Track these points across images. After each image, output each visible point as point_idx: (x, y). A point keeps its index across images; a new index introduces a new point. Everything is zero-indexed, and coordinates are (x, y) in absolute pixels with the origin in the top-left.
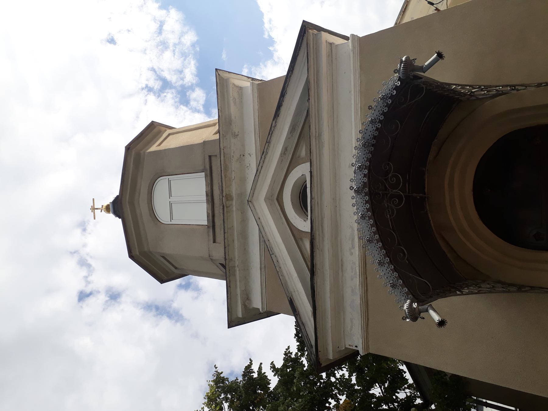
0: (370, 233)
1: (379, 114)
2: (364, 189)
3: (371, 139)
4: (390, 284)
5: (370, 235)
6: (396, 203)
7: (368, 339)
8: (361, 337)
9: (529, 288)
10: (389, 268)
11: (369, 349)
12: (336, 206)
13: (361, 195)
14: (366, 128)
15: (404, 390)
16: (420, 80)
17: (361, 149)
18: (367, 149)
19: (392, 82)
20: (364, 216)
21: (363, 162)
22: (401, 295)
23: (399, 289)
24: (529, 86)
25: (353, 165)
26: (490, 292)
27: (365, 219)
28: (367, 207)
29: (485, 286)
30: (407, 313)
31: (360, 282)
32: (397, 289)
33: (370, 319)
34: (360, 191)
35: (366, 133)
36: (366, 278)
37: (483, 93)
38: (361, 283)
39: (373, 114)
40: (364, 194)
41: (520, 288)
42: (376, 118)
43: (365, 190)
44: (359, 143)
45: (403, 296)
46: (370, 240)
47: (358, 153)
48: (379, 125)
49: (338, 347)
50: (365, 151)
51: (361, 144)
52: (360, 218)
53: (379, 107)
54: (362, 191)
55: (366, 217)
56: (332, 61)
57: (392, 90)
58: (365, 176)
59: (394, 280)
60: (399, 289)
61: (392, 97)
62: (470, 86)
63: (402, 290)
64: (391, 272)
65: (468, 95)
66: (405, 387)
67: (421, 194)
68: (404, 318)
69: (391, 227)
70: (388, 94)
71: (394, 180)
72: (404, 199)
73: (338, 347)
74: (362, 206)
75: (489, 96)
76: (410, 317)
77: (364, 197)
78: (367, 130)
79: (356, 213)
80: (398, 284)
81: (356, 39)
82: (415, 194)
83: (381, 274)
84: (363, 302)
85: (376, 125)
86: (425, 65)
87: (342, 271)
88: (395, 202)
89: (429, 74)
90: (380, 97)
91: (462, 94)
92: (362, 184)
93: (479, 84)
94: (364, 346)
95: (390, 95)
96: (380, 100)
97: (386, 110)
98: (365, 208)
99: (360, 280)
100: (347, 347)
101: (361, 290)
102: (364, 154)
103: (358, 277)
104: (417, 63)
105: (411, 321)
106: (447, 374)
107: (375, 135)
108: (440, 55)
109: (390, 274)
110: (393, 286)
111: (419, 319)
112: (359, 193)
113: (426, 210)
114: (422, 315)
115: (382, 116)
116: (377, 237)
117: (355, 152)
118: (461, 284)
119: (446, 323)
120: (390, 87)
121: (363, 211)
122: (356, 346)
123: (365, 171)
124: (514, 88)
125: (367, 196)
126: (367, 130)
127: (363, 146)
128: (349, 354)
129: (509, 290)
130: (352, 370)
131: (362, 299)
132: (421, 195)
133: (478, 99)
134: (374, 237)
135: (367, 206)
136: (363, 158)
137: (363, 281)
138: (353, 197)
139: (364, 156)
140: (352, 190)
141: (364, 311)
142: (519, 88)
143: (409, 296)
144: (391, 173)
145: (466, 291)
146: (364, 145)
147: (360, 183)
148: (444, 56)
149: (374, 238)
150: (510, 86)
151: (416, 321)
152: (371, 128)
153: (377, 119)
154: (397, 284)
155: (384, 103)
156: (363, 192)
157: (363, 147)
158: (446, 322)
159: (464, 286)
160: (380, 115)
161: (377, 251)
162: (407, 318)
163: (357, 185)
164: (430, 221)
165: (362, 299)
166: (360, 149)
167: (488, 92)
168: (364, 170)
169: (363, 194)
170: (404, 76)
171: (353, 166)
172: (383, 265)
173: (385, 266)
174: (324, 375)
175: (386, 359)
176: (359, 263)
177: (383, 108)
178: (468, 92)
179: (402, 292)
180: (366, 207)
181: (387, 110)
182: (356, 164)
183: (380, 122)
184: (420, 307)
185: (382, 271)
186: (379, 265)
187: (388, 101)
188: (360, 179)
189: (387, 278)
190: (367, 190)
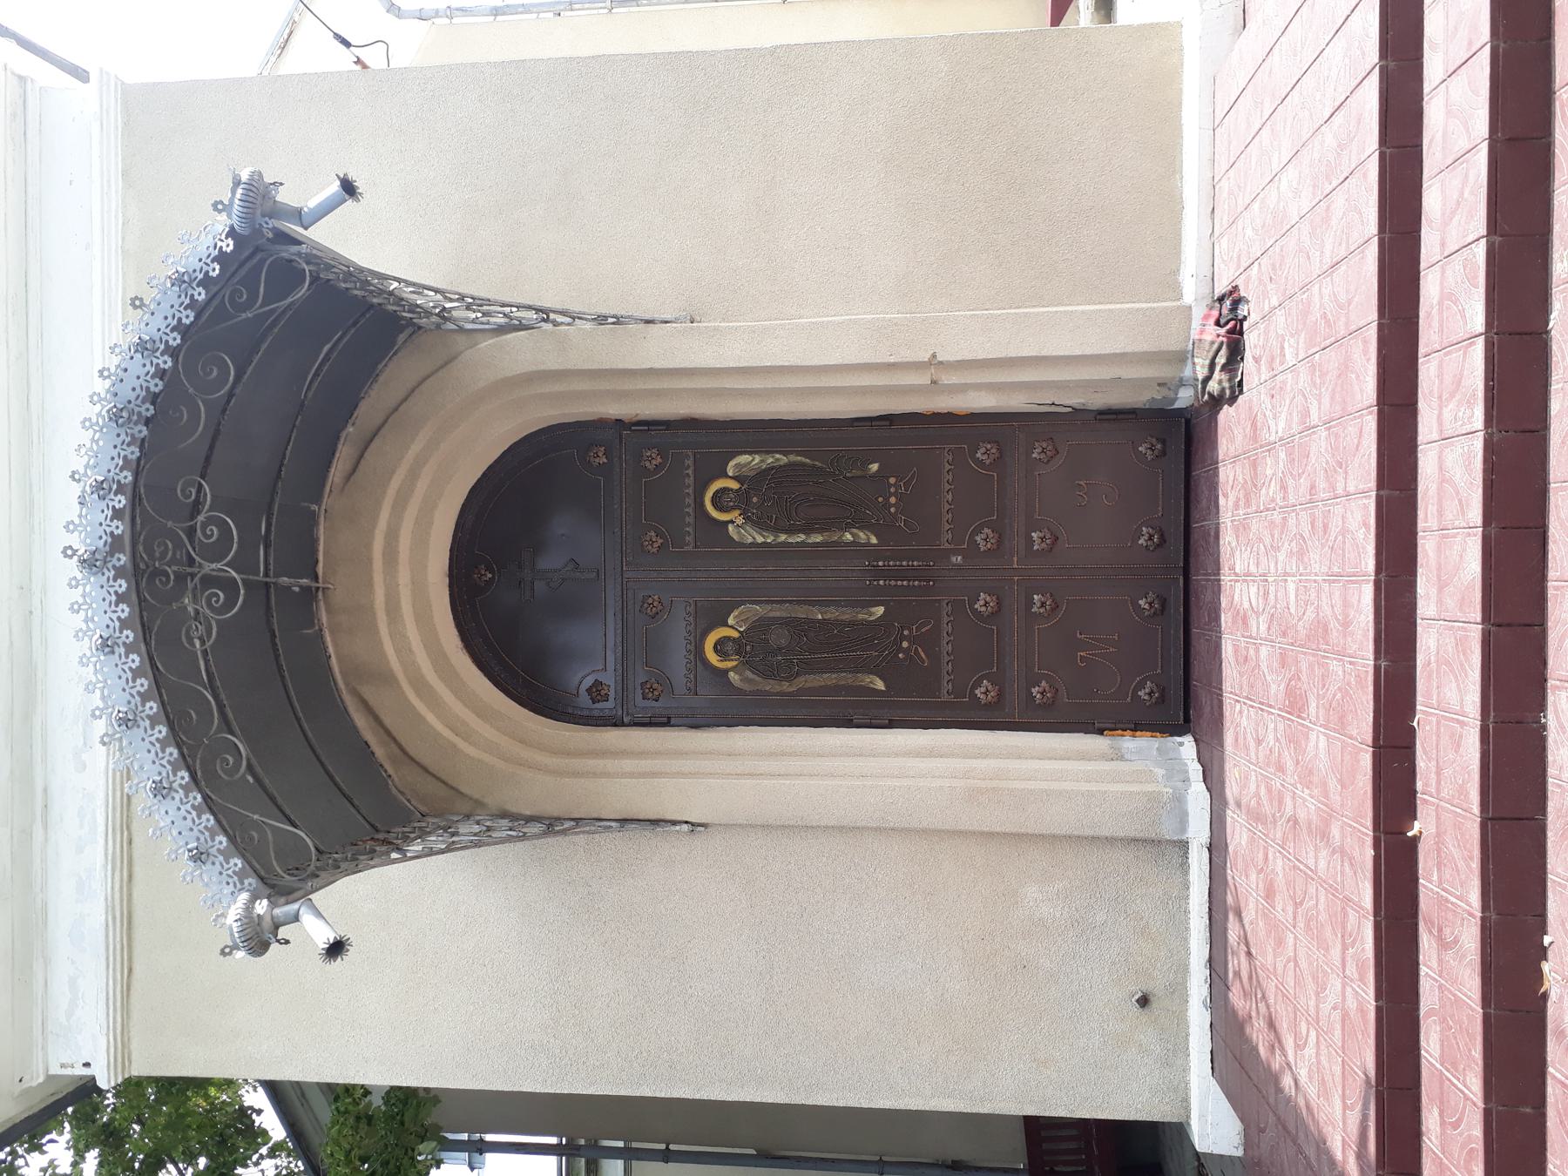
0: (129, 697)
1: (165, 325)
2: (112, 556)
3: (139, 402)
4: (190, 851)
5: (129, 702)
6: (217, 602)
7: (129, 1032)
8: (105, 1032)
9: (572, 823)
10: (187, 803)
11: (130, 1062)
12: (31, 612)
13: (103, 574)
14: (123, 366)
15: (257, 1164)
16: (295, 249)
17: (105, 430)
18: (126, 432)
19: (210, 236)
20: (109, 643)
21: (109, 471)
22: (220, 883)
23: (217, 863)
24: (580, 318)
25: (77, 477)
26: (477, 845)
27: (113, 652)
28: (120, 614)
29: (467, 829)
30: (236, 935)
31: (106, 854)
32: (209, 865)
33: (137, 968)
34: (98, 563)
35: (122, 381)
36: (130, 842)
37: (473, 316)
38: (110, 858)
39: (147, 324)
40: (113, 572)
41: (552, 825)
42: (157, 338)
43: (114, 561)
44: (98, 407)
45: (228, 883)
46: (129, 720)
47: (93, 440)
48: (167, 362)
49: (21, 1081)
50: (118, 435)
51: (104, 412)
52: (97, 649)
53: (165, 306)
54: (105, 562)
55: (116, 647)
56: (25, 134)
57: (209, 261)
58: (117, 514)
59: (202, 839)
60: (217, 863)
61: (206, 282)
62: (436, 291)
63: (226, 866)
64: (194, 813)
65: (436, 315)
66: (261, 1155)
67: (305, 580)
68: (227, 950)
69: (205, 677)
70: (195, 271)
71: (212, 534)
72: (242, 592)
73: (21, 1081)
74: (106, 612)
75: (491, 327)
76: (245, 944)
77: (111, 581)
78: (126, 370)
79: (85, 633)
80: (213, 851)
81: (113, 83)
82: (285, 580)
83: (162, 824)
84: (114, 918)
85: (155, 361)
86: (306, 206)
87: (45, 826)
88: (214, 599)
89: (323, 235)
90: (170, 277)
91: (418, 310)
92: (106, 542)
93: (461, 291)
94: (112, 1060)
95: (201, 276)
96: (169, 285)
97: (188, 318)
98: (114, 616)
99: (106, 849)
100: (54, 1073)
101: (109, 880)
102: (115, 447)
103: (102, 841)
104: (284, 197)
105: (248, 956)
106: (370, 1090)
107: (153, 389)
108: (349, 188)
109: (189, 822)
110: (199, 857)
111: (274, 947)
112: (94, 569)
113: (319, 626)
114: (283, 932)
115: (175, 334)
116: (151, 708)
117: (86, 437)
118: (406, 830)
119: (349, 947)
120: (202, 251)
121: (108, 626)
122: (87, 1065)
123: (117, 499)
124: (545, 316)
125: (123, 581)
126: (126, 370)
127: (111, 419)
128: (64, 1093)
129: (525, 833)
130: (81, 1146)
131: (113, 909)
132: (304, 581)
133: (461, 330)
134: (140, 708)
135: (123, 611)
136: (113, 459)
137: (118, 850)
138: (74, 583)
139: (115, 453)
140: (71, 557)
141: (118, 947)
142: (558, 320)
143: (246, 882)
144: (205, 511)
145: (416, 847)
146: (115, 417)
147: (101, 538)
148: (360, 191)
149: (141, 712)
150: (538, 310)
151: (264, 954)
152: (141, 368)
153: (158, 342)
154: (210, 850)
155: (183, 296)
156: (110, 565)
157: (111, 423)
158: (349, 945)
159: (412, 835)
160: (168, 331)
161: (149, 751)
162: (235, 947)
163: (88, 541)
164: (330, 656)
165: (113, 909)
166: (102, 430)
167: (484, 314)
168: (113, 497)
169: (109, 570)
170: (243, 225)
171: (74, 479)
172: (168, 794)
173: (173, 798)
174: (564, 1142)
175: (200, 1084)
176: (108, 794)
177: (179, 311)
178: (434, 307)
179: (225, 873)
180: (116, 615)
181: (192, 319)
182: (85, 474)
183: (173, 352)
184: (278, 911)
185: (163, 812)
186: (155, 796)
187: (196, 294)
188: (101, 524)
189: (180, 833)
190: (123, 559)
